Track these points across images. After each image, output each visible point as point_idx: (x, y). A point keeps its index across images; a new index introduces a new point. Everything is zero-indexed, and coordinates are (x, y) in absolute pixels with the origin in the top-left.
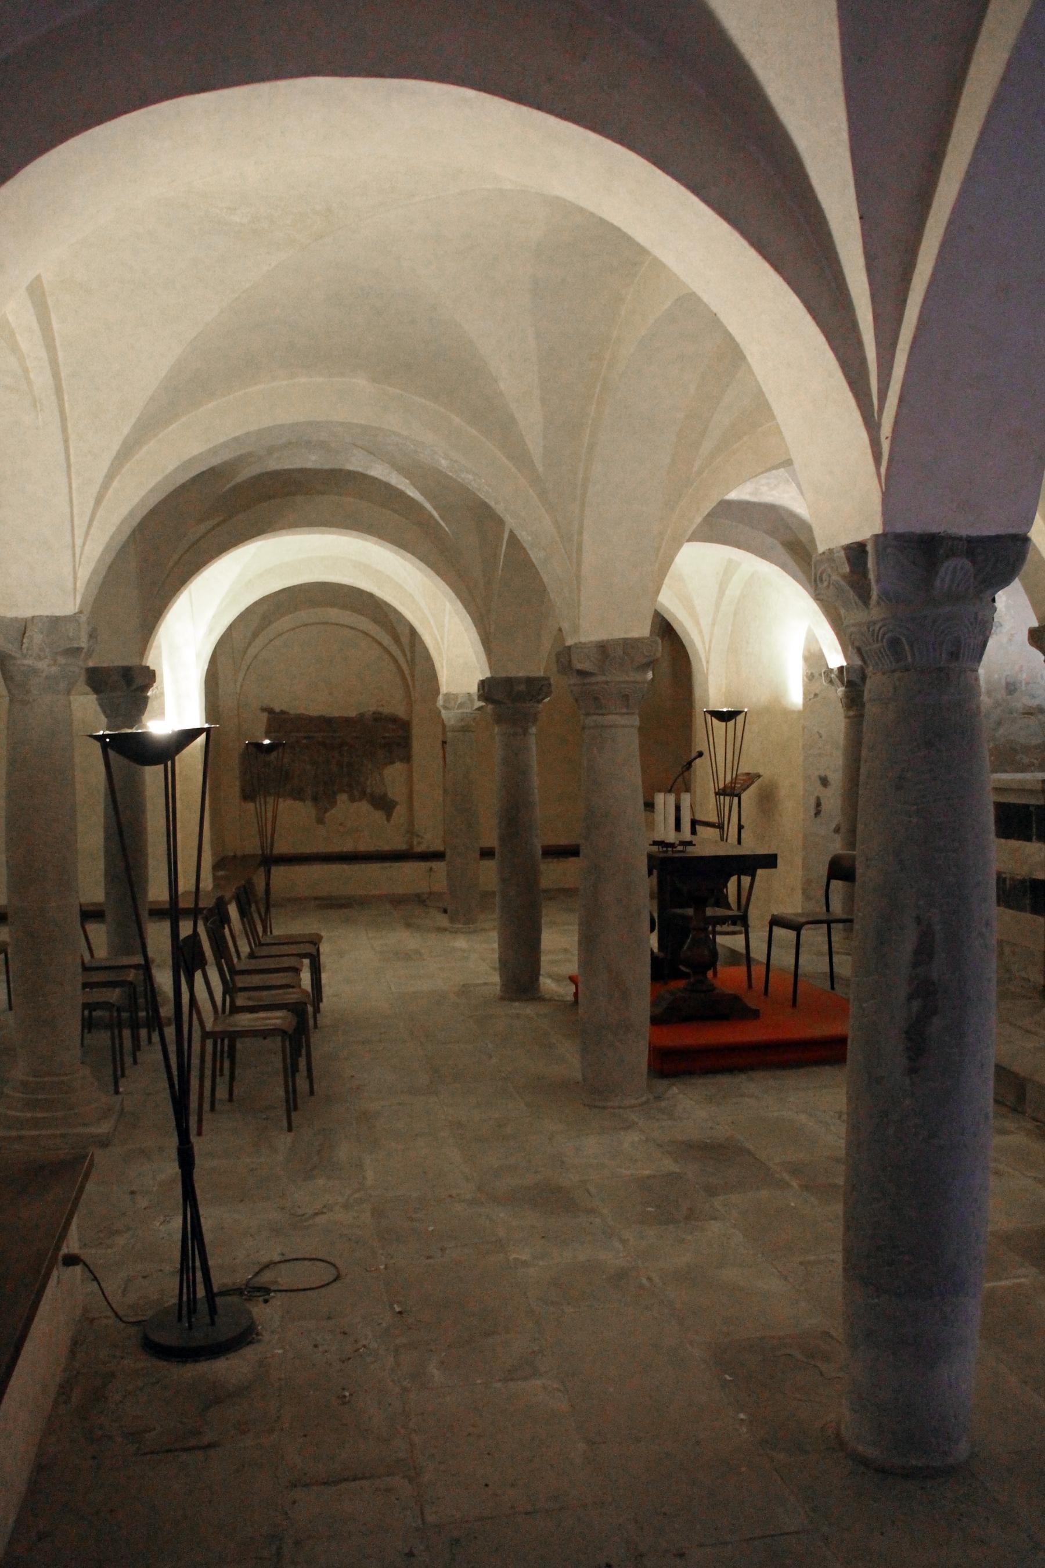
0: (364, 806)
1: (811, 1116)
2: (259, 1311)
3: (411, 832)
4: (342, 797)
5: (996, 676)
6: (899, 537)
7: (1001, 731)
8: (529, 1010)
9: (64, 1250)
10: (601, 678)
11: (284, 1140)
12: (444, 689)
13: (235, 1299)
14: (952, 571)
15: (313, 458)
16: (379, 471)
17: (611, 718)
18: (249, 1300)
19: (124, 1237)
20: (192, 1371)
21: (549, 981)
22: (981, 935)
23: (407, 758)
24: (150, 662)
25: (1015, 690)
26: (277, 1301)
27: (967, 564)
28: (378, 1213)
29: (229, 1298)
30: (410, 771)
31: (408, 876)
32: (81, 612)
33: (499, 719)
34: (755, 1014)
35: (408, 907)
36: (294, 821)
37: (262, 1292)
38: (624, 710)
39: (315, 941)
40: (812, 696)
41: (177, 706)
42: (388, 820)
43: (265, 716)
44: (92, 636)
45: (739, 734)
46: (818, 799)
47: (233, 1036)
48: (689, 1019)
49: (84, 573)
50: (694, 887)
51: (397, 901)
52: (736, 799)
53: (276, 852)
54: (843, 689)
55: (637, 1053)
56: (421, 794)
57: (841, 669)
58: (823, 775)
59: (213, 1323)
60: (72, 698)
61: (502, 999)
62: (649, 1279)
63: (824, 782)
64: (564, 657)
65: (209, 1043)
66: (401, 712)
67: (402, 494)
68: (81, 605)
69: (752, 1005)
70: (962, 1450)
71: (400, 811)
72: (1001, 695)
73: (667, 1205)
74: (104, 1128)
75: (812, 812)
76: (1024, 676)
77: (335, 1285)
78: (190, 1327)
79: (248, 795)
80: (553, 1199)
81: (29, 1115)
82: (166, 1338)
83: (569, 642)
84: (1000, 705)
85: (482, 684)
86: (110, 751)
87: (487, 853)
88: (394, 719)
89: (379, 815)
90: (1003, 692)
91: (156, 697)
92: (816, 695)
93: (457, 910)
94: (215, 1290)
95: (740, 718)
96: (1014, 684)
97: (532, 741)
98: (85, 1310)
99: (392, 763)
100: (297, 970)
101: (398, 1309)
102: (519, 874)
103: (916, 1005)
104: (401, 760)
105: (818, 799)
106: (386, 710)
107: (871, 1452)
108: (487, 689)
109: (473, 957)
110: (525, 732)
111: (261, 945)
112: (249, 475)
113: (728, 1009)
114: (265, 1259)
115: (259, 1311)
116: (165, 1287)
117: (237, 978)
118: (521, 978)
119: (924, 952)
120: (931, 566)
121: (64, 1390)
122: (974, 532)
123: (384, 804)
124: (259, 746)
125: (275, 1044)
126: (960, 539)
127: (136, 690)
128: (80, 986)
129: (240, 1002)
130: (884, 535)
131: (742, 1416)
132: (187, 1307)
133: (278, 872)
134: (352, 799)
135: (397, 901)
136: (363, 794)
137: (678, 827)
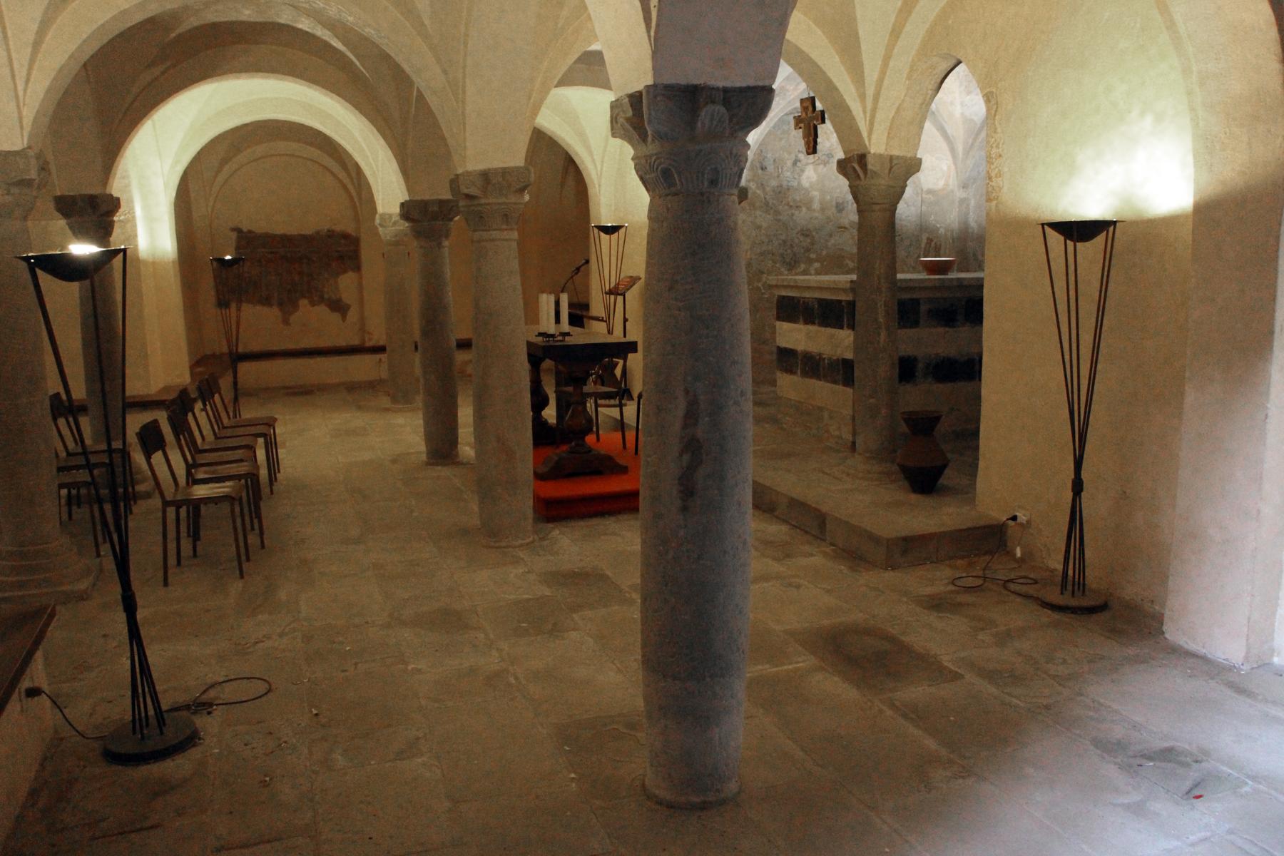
0: (322, 310)
1: (618, 546)
2: (200, 721)
3: (363, 329)
4: (304, 303)
6: (668, 87)
8: (444, 472)
9: (26, 684)
10: (483, 201)
11: (236, 587)
12: (380, 209)
13: (185, 713)
14: (709, 114)
15: (247, 12)
16: (304, 24)
17: (494, 234)
18: (195, 713)
19: (83, 673)
20: (144, 771)
21: (467, 448)
22: (737, 403)
23: (358, 268)
24: (115, 189)
26: (218, 712)
27: (723, 110)
28: (308, 639)
29: (180, 713)
30: (361, 278)
31: (361, 368)
32: (29, 147)
33: (417, 234)
34: (624, 470)
35: (356, 392)
36: (259, 323)
37: (203, 706)
38: (504, 227)
39: (271, 423)
41: (151, 231)
42: (286, 322)
43: (234, 235)
44: (44, 168)
45: (621, 242)
47: (196, 506)
48: (571, 475)
49: (29, 115)
50: (575, 366)
51: (352, 387)
52: (620, 299)
53: (240, 350)
55: (525, 504)
56: (371, 296)
59: (162, 733)
60: (29, 223)
61: (428, 464)
62: (516, 678)
64: (454, 182)
65: (171, 511)
66: (350, 228)
67: (327, 45)
68: (29, 140)
69: (622, 462)
70: (732, 787)
71: (353, 315)
72: (832, 211)
73: (537, 620)
74: (83, 585)
77: (270, 696)
78: (143, 738)
79: (222, 304)
80: (450, 621)
81: (14, 579)
82: (128, 748)
83: (460, 171)
85: (402, 205)
86: (39, 272)
87: (464, 345)
88: (345, 236)
89: (335, 317)
90: (834, 210)
91: (127, 221)
93: (392, 391)
94: (164, 708)
95: (622, 231)
97: (446, 251)
98: (56, 732)
99: (345, 272)
100: (251, 448)
101: (315, 712)
102: (438, 365)
103: (686, 458)
104: (353, 270)
106: (339, 228)
107: (662, 793)
108: (408, 211)
109: (406, 431)
110: (440, 245)
111: (224, 428)
112: (188, 27)
113: (605, 466)
114: (209, 681)
115: (200, 721)
116: (120, 709)
117: (197, 456)
118: (442, 448)
119: (691, 416)
120: (694, 112)
121: (33, 793)
122: (728, 84)
123: (338, 307)
124: (222, 261)
125: (225, 508)
126: (718, 89)
127: (102, 215)
128: (55, 470)
129: (200, 476)
130: (655, 86)
131: (573, 775)
132: (138, 723)
133: (244, 367)
134: (313, 304)
135: (352, 387)
136: (322, 300)
137: (558, 320)
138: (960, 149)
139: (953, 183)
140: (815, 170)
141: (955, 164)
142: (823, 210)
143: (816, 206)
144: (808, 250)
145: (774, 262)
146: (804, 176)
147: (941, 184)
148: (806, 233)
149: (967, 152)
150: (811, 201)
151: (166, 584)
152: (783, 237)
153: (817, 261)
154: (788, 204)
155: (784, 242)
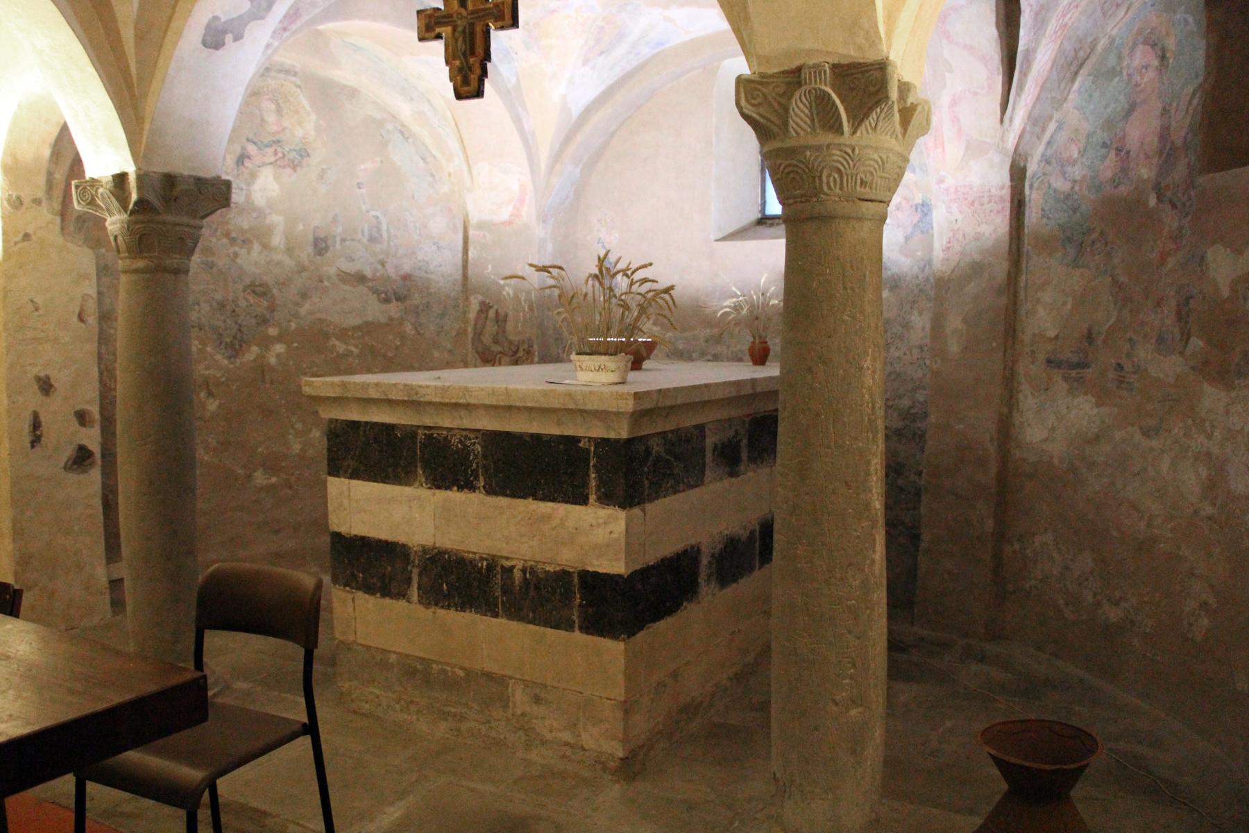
5: (301, 227)
7: (307, 306)
25: (326, 249)
40: (20, 237)
46: (36, 416)
54: (125, 216)
57: (121, 179)
58: (42, 374)
63: (46, 386)
75: (27, 440)
76: (340, 230)
79: (636, 394)
84: (304, 269)
90: (310, 250)
92: (27, 237)
96: (325, 240)
105: (36, 416)
138: (544, 156)
139: (528, 213)
140: (276, 178)
141: (533, 181)
142: (289, 250)
143: (277, 240)
144: (264, 321)
145: (203, 343)
146: (257, 186)
147: (505, 214)
148: (259, 289)
149: (557, 158)
150: (270, 230)
151: (651, 264)
152: (218, 297)
153: (279, 339)
154: (227, 235)
155: (222, 305)
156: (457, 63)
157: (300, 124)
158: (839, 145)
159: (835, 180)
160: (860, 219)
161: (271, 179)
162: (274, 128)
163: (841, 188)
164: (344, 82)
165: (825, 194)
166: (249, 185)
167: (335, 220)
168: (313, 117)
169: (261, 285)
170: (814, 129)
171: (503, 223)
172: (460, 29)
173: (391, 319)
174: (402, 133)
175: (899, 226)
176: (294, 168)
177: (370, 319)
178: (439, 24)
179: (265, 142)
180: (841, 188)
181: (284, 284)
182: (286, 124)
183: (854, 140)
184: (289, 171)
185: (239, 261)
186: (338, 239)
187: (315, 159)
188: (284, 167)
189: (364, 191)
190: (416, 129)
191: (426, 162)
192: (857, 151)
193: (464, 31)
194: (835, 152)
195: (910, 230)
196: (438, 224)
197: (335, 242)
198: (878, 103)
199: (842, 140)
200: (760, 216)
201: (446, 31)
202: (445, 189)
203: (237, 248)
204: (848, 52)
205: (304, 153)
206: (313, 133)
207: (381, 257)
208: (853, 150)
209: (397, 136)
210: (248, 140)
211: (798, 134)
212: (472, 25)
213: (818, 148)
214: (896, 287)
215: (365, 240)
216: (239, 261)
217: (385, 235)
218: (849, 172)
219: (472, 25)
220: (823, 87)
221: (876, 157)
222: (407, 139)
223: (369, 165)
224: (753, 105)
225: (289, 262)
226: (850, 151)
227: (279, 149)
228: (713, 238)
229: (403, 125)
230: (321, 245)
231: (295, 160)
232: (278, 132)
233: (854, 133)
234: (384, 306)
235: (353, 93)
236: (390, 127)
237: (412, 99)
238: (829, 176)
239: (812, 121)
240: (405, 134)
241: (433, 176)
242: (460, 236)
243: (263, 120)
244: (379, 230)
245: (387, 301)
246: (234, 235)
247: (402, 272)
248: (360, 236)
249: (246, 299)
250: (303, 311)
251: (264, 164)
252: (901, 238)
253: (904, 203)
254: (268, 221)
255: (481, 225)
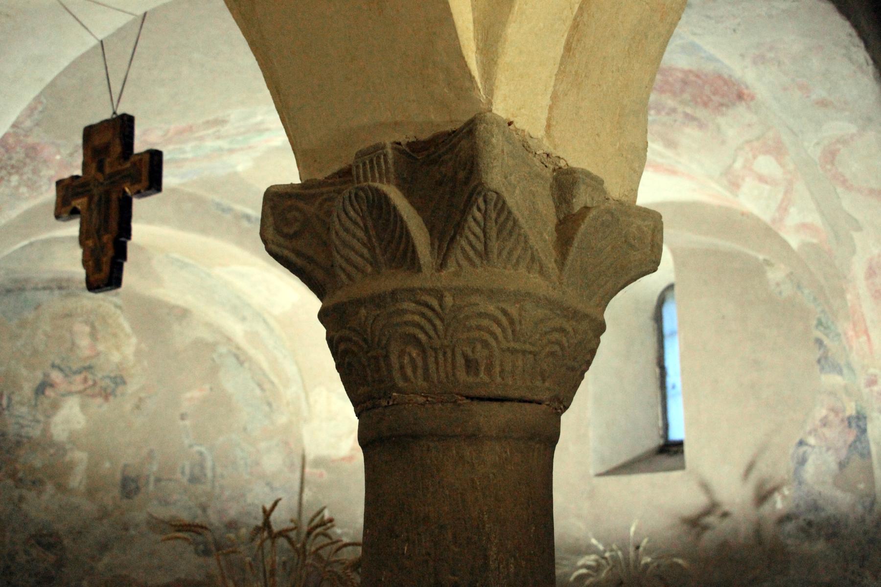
5: (107, 465)
7: (106, 560)
25: (138, 489)
76: (155, 468)
96: (135, 480)
140: (83, 407)
142: (91, 492)
143: (77, 480)
150: (70, 467)
154: (13, 475)
156: (90, 243)
157: (118, 348)
158: (412, 291)
159: (412, 360)
160: (474, 437)
161: (77, 409)
162: (87, 353)
163: (427, 377)
164: (173, 301)
165: (399, 391)
166: (48, 417)
167: (151, 455)
168: (134, 340)
169: (51, 535)
170: (374, 263)
171: (343, 459)
172: (96, 199)
173: (209, 576)
174: (237, 357)
175: (828, 449)
176: (106, 398)
177: (183, 576)
178: (77, 195)
179: (75, 367)
180: (427, 377)
181: (79, 534)
182: (101, 347)
183: (444, 279)
184: (99, 400)
185: (24, 506)
186: (152, 479)
187: (132, 387)
188: (93, 396)
189: (187, 423)
190: (252, 352)
191: (263, 389)
192: (449, 300)
193: (100, 200)
194: (405, 305)
195: (844, 453)
196: (273, 462)
197: (147, 483)
198: (469, 203)
199: (416, 282)
200: (661, 442)
201: (80, 203)
202: (282, 420)
203: (24, 492)
204: (426, 118)
205: (119, 380)
206: (131, 358)
207: (204, 499)
208: (441, 298)
209: (231, 361)
210: (53, 366)
211: (349, 276)
212: (108, 193)
213: (377, 300)
214: (835, 535)
215: (185, 480)
216: (24, 506)
217: (209, 474)
218: (437, 343)
219: (108, 193)
220: (377, 184)
221: (491, 308)
222: (241, 363)
223: (196, 394)
224: (286, 236)
225: (88, 507)
226: (435, 303)
227: (90, 376)
228: (592, 472)
229: (238, 348)
230: (130, 486)
231: (110, 387)
232: (89, 358)
233: (442, 266)
234: (201, 560)
235: (183, 314)
236: (223, 350)
237: (244, 319)
238: (402, 354)
239: (372, 249)
240: (240, 358)
241: (269, 404)
242: (298, 475)
243: (73, 344)
244: (202, 467)
245: (206, 553)
246: (20, 475)
247: (226, 519)
248: (178, 475)
249: (26, 552)
250: (100, 566)
251: (70, 393)
252: (831, 461)
253: (832, 416)
254: (67, 458)
255: (319, 462)
